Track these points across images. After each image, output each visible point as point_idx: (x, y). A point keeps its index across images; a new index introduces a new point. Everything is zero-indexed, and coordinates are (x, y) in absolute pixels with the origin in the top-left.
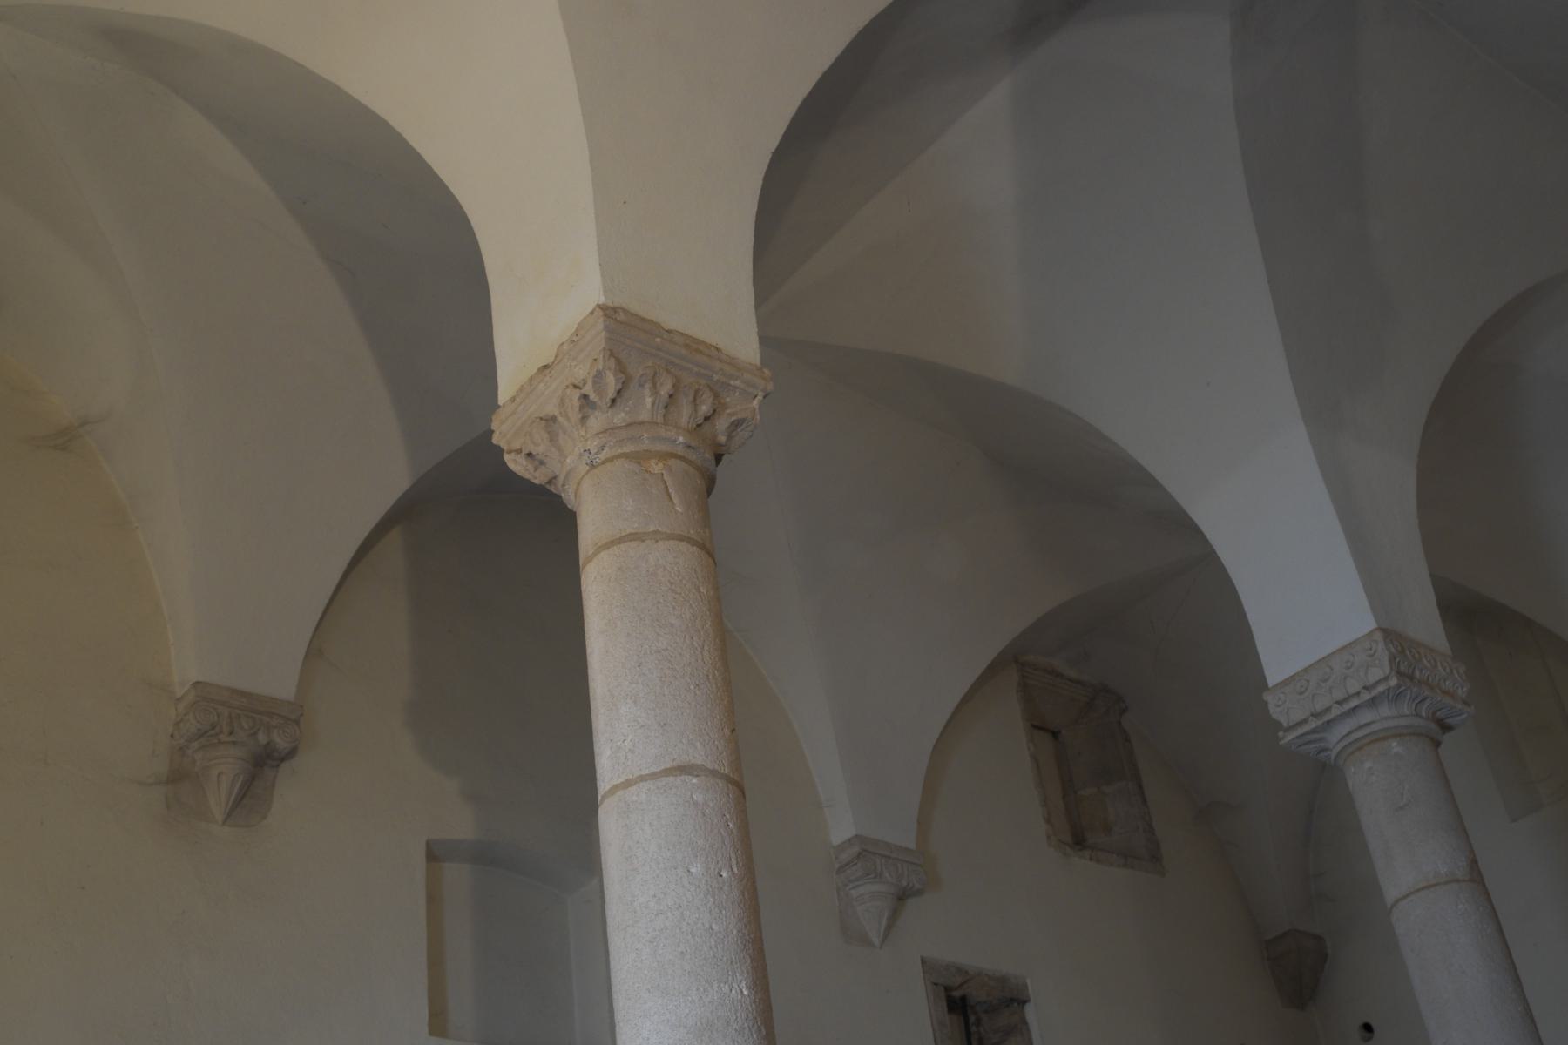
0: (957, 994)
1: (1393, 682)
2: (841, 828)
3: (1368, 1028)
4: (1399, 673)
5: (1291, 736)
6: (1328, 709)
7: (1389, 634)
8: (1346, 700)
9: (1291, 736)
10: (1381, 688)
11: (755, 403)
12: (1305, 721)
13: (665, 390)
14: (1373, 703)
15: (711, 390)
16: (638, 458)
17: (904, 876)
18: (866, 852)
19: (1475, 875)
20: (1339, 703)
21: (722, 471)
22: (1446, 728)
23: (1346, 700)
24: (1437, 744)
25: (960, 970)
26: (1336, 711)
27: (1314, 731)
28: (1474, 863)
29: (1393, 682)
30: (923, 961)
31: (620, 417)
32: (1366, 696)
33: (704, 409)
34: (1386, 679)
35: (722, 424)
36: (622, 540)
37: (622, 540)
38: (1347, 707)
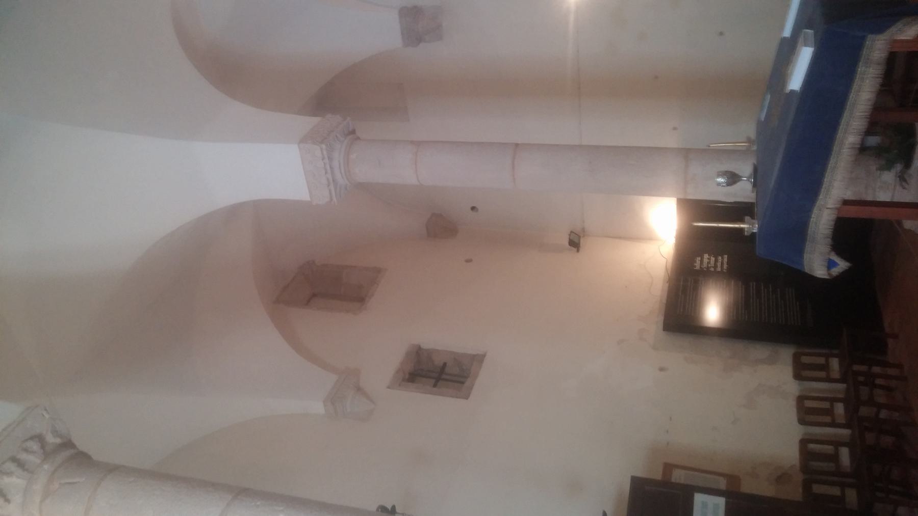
0: (407, 377)
1: (324, 146)
2: (318, 408)
3: (473, 208)
4: (322, 142)
5: (335, 199)
6: (328, 179)
7: (303, 141)
8: (326, 170)
9: (335, 199)
10: (325, 153)
11: (47, 416)
12: (330, 191)
13: (12, 466)
14: (330, 159)
15: (27, 440)
16: (46, 494)
17: (348, 384)
18: (334, 399)
19: (418, 144)
20: (326, 173)
21: (82, 444)
22: (353, 132)
23: (326, 170)
24: (358, 138)
25: (398, 372)
26: (330, 176)
27: (336, 189)
28: (412, 142)
29: (324, 146)
30: (388, 387)
31: (17, 499)
32: (327, 161)
33: (34, 446)
34: (322, 149)
35: (51, 439)
36: (513, 168)
37: (513, 168)
38: (329, 171)
